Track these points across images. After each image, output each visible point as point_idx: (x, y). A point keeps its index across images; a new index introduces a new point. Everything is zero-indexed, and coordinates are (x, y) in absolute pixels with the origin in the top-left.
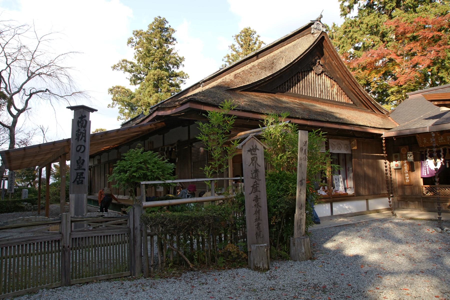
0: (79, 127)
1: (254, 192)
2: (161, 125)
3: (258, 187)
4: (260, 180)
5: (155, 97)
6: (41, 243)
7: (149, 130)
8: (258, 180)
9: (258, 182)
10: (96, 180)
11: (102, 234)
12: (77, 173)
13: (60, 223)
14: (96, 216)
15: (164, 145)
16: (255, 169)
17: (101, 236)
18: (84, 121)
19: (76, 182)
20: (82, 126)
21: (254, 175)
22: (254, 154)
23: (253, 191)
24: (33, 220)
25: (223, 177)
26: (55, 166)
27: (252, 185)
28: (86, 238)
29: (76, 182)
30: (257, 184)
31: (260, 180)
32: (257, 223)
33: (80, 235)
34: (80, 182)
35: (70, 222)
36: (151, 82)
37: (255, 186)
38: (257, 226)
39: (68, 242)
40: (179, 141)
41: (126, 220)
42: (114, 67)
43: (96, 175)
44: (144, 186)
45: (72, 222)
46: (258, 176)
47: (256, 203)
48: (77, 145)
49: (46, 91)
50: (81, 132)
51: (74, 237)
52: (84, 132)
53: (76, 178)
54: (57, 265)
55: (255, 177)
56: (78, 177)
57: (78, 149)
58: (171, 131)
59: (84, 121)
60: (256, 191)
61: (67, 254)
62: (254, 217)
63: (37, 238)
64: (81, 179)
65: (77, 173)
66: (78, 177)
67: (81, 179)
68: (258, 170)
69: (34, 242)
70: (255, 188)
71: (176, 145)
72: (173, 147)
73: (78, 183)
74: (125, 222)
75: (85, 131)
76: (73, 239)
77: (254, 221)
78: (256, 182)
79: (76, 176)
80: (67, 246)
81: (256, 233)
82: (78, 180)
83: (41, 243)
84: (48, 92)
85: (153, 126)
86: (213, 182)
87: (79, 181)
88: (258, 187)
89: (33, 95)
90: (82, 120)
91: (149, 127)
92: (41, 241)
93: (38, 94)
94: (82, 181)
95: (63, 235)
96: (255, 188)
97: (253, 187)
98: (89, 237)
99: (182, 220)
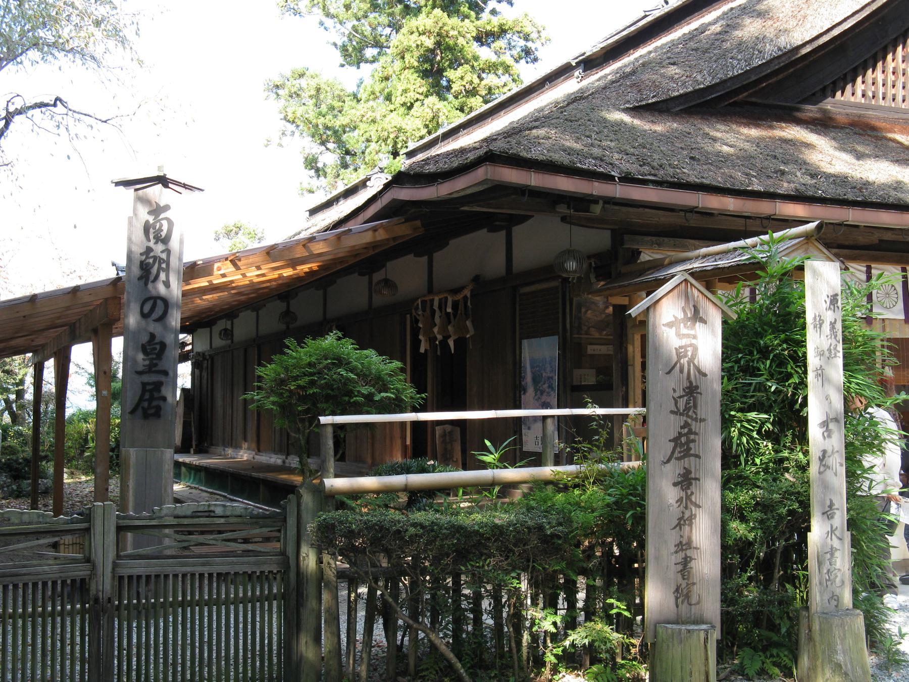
0: (149, 240)
1: (678, 459)
2: (404, 230)
3: (694, 441)
4: (702, 420)
5: (422, 112)
6: (35, 585)
7: (373, 245)
8: (696, 420)
9: (694, 426)
10: (219, 402)
11: (206, 570)
12: (144, 385)
13: (88, 530)
14: (189, 513)
15: (430, 290)
16: (686, 384)
17: (201, 575)
18: (165, 223)
19: (140, 412)
20: (158, 239)
21: (682, 403)
22: (688, 336)
23: (676, 455)
24: (14, 520)
25: (416, 424)
26: (82, 355)
27: (673, 435)
28: (157, 576)
29: (140, 412)
30: (690, 432)
31: (702, 420)
32: (681, 555)
33: (139, 568)
34: (152, 411)
35: (113, 529)
36: (412, 60)
37: (683, 440)
38: (680, 567)
39: (108, 587)
40: (476, 279)
41: (279, 531)
42: (114, 264)
43: (218, 386)
44: (330, 430)
45: (120, 529)
46: (695, 406)
47: (683, 494)
48: (144, 297)
49: (55, 105)
50: (155, 258)
51: (125, 572)
52: (164, 256)
53: (141, 399)
54: (78, 648)
55: (687, 409)
56: (147, 396)
57: (147, 308)
58: (453, 243)
59: (165, 223)
60: (687, 453)
61: (104, 621)
62: (672, 538)
63: (24, 571)
64: (155, 403)
65: (144, 385)
66: (147, 396)
67: (155, 403)
68: (697, 387)
69: (14, 579)
70: (682, 445)
71: (467, 292)
72: (459, 297)
73: (146, 416)
74: (277, 534)
75: (168, 252)
76: (121, 578)
77: (673, 549)
78: (686, 425)
79: (139, 392)
80: (106, 598)
81: (677, 590)
82: (146, 404)
83: (35, 585)
84: (60, 108)
85: (381, 235)
86: (549, 421)
87: (150, 407)
88: (694, 441)
89: (17, 119)
90: (157, 220)
91: (368, 238)
92: (33, 578)
93: (30, 113)
94: (159, 408)
95: (94, 567)
96: (682, 445)
97: (675, 440)
98: (166, 576)
99: (436, 537)
